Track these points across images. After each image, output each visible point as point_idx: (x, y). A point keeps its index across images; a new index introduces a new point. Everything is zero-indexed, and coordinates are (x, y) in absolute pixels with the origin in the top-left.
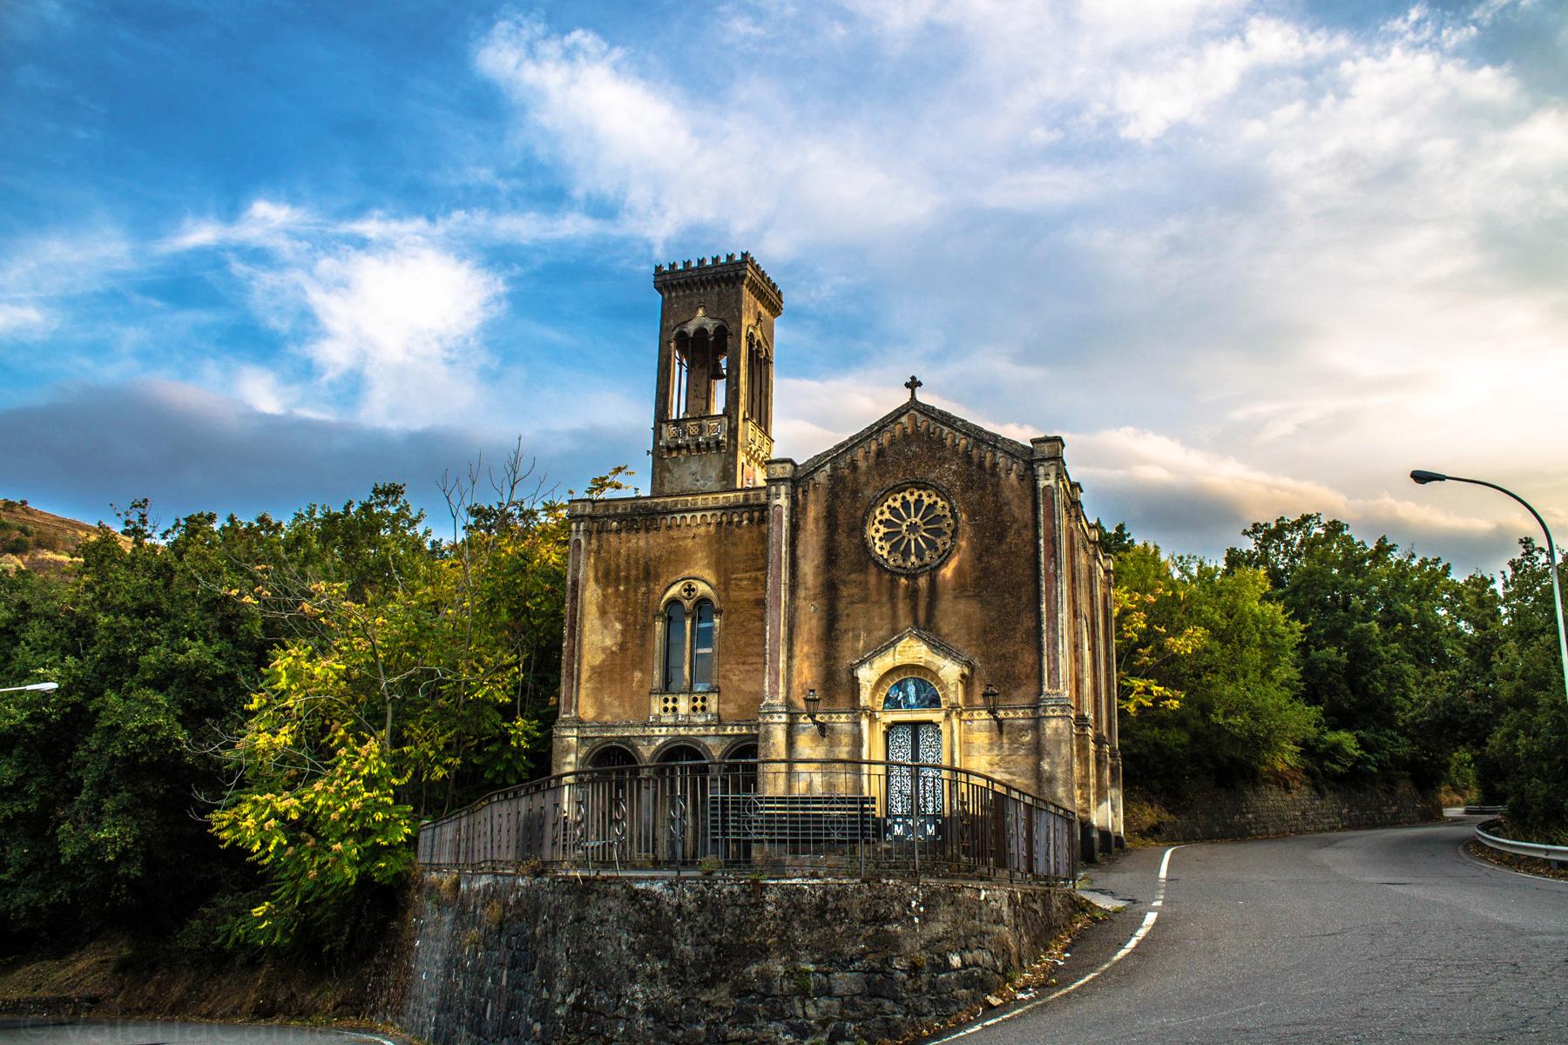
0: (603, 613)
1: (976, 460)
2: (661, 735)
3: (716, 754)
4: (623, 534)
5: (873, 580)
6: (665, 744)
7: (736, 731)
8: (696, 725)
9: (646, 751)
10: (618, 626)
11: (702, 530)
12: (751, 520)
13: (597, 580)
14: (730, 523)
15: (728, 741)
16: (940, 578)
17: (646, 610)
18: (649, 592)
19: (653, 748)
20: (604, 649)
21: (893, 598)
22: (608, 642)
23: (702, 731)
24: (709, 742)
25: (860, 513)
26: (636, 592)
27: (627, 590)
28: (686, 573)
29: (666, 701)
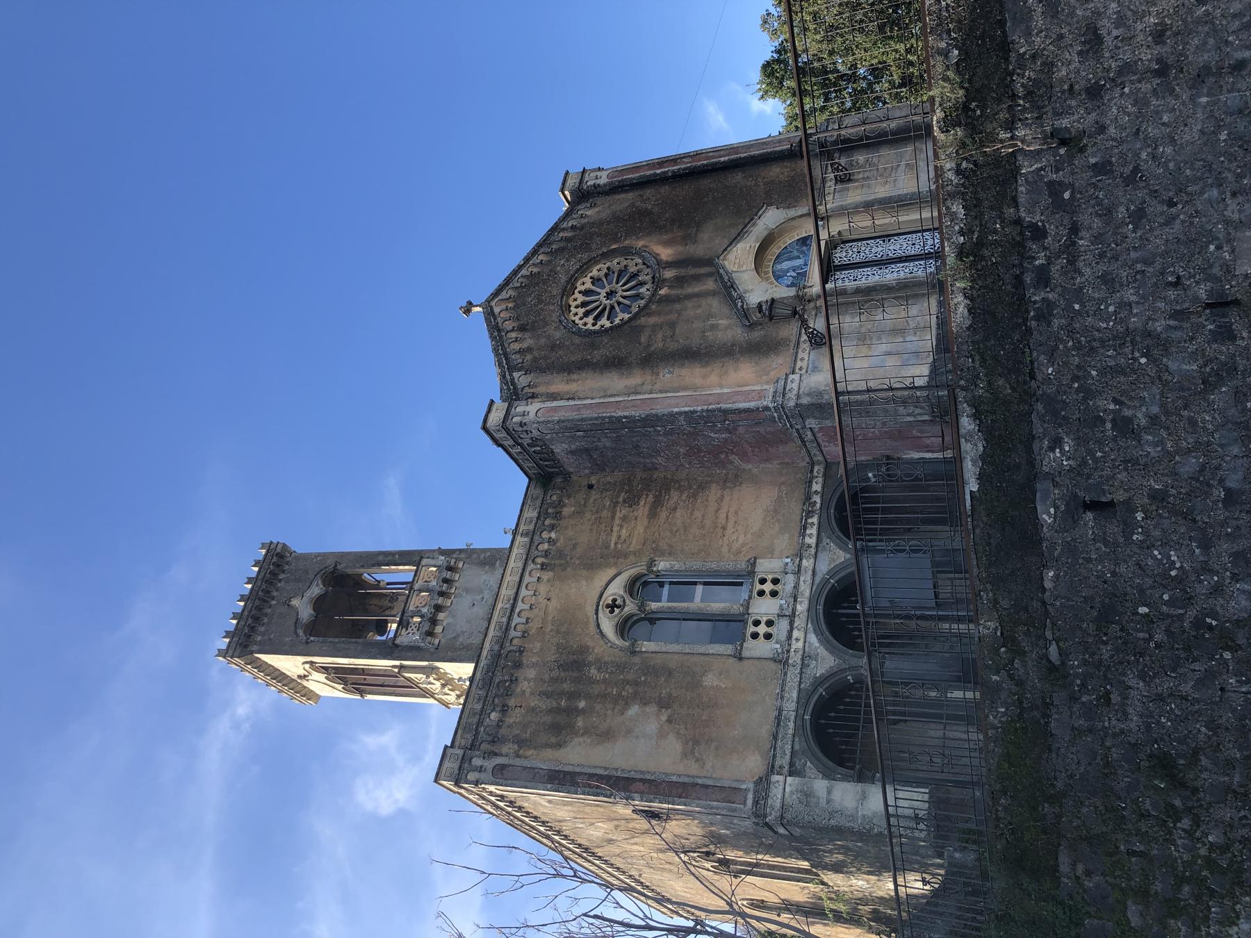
0: (607, 736)
1: (562, 244)
2: (806, 639)
3: (841, 556)
4: (512, 702)
5: (653, 320)
6: (818, 632)
7: (813, 531)
8: (796, 587)
9: (825, 661)
10: (634, 710)
11: (543, 589)
12: (552, 527)
13: (559, 746)
14: (546, 554)
15: (826, 541)
16: (670, 259)
17: (621, 667)
18: (601, 665)
19: (822, 651)
20: (661, 735)
21: (678, 299)
22: (652, 727)
23: (806, 577)
24: (824, 567)
25: (577, 340)
26: (593, 682)
27: (588, 697)
28: (590, 610)
29: (755, 636)
